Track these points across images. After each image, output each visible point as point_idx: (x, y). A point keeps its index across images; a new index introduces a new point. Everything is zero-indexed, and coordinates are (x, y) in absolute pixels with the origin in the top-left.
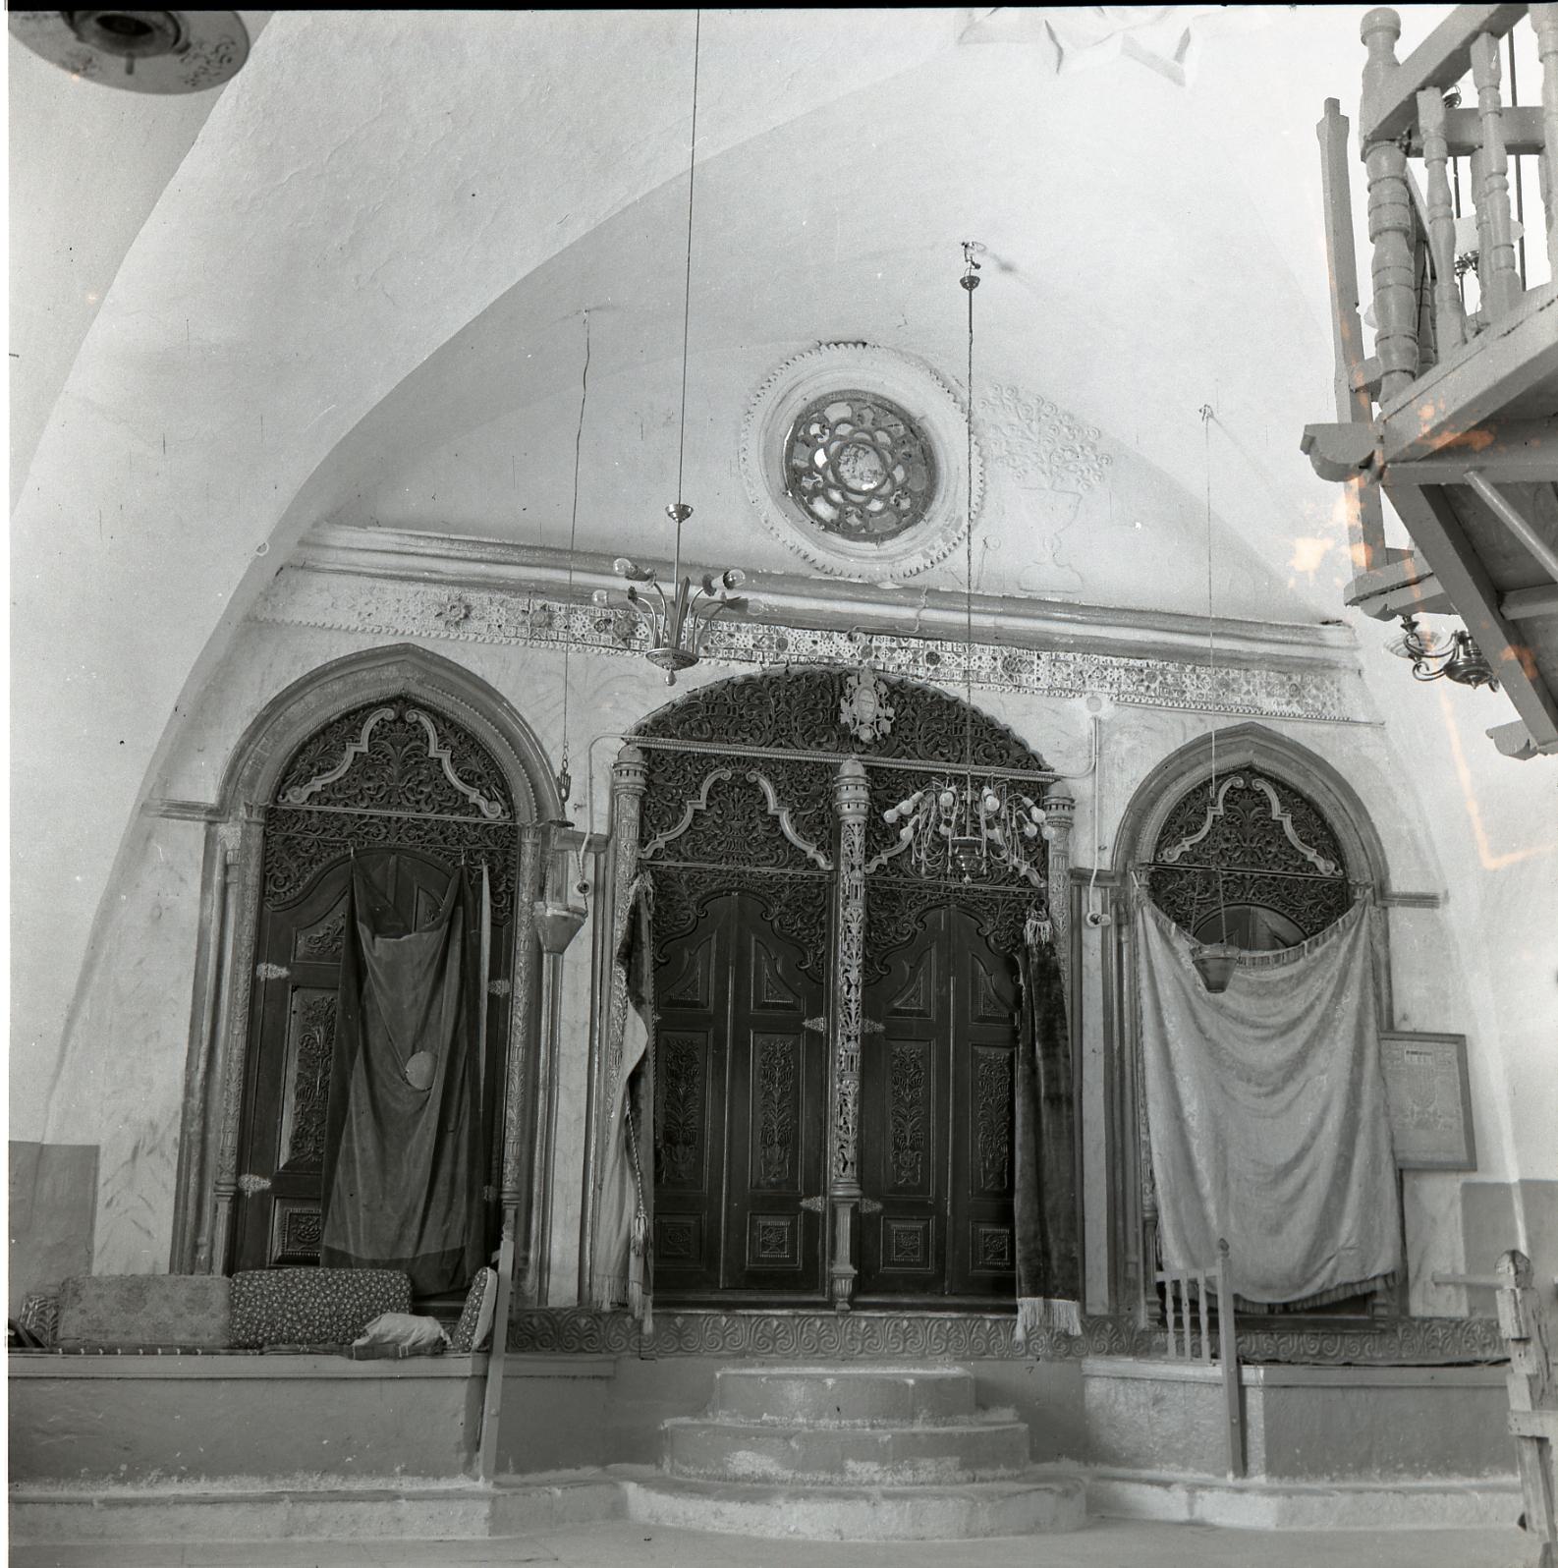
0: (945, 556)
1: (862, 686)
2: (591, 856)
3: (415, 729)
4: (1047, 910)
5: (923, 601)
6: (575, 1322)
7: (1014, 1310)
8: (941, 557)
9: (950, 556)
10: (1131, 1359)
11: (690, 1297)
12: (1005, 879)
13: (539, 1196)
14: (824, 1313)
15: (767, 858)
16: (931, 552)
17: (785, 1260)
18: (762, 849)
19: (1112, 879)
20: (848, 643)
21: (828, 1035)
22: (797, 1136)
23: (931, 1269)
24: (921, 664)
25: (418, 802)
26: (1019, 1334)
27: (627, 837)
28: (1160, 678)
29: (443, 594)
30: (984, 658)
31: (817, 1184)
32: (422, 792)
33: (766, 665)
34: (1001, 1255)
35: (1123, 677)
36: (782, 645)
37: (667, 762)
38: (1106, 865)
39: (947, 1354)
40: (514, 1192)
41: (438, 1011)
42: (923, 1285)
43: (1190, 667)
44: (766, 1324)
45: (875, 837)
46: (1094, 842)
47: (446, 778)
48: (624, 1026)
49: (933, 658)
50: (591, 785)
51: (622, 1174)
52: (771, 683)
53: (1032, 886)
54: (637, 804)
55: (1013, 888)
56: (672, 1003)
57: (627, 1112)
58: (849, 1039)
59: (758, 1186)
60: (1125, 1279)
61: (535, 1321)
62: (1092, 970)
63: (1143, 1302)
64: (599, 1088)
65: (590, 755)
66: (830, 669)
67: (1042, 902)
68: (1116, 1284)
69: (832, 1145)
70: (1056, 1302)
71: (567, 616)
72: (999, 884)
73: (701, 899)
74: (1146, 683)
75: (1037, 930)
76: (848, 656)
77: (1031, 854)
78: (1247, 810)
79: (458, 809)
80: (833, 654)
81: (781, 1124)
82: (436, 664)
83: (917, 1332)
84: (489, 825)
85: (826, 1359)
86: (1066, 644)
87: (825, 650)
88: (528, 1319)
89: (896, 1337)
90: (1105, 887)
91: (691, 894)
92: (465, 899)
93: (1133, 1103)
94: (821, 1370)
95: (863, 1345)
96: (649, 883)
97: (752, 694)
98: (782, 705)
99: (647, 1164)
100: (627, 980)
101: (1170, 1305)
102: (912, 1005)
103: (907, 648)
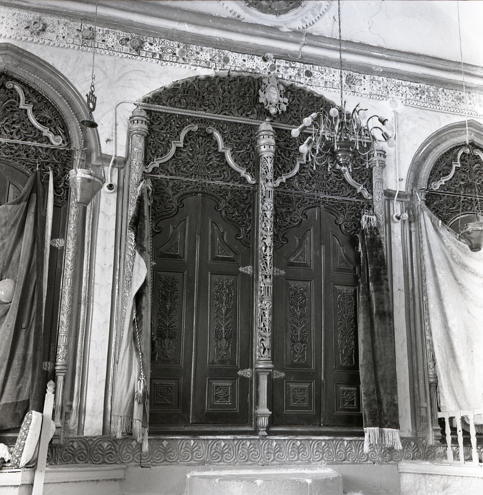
0: (313, 23)
1: (271, 84)
2: (116, 170)
3: (12, 93)
4: (373, 210)
5: (304, 40)
6: (101, 445)
7: (362, 434)
8: (311, 23)
9: (316, 24)
10: (428, 463)
11: (172, 429)
12: (349, 194)
13: (80, 368)
14: (252, 437)
15: (218, 176)
16: (306, 20)
17: (228, 406)
18: (215, 171)
19: (406, 196)
20: (263, 62)
21: (253, 276)
22: (235, 334)
23: (313, 411)
24: (302, 76)
25: (11, 133)
26: (366, 449)
27: (137, 160)
28: (427, 93)
29: (32, 16)
30: (335, 76)
31: (247, 362)
32: (14, 128)
33: (218, 71)
34: (352, 402)
35: (408, 92)
36: (226, 60)
37: (159, 117)
38: (403, 189)
39: (323, 461)
40: (63, 365)
41: (18, 256)
42: (308, 420)
43: (441, 89)
44: (217, 445)
45: (278, 167)
46: (396, 175)
47: (29, 121)
48: (133, 266)
49: (308, 74)
50: (116, 129)
51: (131, 354)
52: (220, 81)
53: (364, 198)
54: (143, 140)
55: (354, 199)
56: (163, 256)
57: (134, 317)
58: (266, 277)
59: (213, 363)
60: (420, 416)
61: (75, 445)
62: (397, 245)
63: (431, 429)
64: (118, 304)
65: (116, 112)
66: (253, 75)
67: (370, 207)
68: (415, 419)
69: (257, 339)
70: (386, 430)
71: (103, 35)
72: (346, 197)
73: (180, 197)
74: (420, 95)
75: (369, 220)
76: (262, 69)
77: (363, 181)
78: (472, 165)
79: (36, 139)
80: (254, 68)
81: (226, 327)
82: (26, 57)
83: (305, 448)
84: (54, 149)
85: (254, 465)
86: (378, 72)
87: (249, 64)
88: (71, 443)
89: (294, 451)
90: (402, 201)
91: (174, 194)
92: (37, 190)
93: (421, 319)
94: (250, 472)
95: (274, 456)
96: (149, 185)
97: (210, 86)
98: (226, 93)
99: (146, 347)
100: (135, 239)
101: (448, 431)
102: (301, 260)
103: (294, 68)
